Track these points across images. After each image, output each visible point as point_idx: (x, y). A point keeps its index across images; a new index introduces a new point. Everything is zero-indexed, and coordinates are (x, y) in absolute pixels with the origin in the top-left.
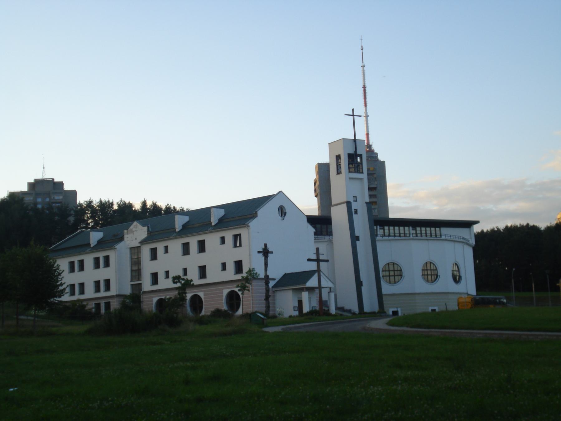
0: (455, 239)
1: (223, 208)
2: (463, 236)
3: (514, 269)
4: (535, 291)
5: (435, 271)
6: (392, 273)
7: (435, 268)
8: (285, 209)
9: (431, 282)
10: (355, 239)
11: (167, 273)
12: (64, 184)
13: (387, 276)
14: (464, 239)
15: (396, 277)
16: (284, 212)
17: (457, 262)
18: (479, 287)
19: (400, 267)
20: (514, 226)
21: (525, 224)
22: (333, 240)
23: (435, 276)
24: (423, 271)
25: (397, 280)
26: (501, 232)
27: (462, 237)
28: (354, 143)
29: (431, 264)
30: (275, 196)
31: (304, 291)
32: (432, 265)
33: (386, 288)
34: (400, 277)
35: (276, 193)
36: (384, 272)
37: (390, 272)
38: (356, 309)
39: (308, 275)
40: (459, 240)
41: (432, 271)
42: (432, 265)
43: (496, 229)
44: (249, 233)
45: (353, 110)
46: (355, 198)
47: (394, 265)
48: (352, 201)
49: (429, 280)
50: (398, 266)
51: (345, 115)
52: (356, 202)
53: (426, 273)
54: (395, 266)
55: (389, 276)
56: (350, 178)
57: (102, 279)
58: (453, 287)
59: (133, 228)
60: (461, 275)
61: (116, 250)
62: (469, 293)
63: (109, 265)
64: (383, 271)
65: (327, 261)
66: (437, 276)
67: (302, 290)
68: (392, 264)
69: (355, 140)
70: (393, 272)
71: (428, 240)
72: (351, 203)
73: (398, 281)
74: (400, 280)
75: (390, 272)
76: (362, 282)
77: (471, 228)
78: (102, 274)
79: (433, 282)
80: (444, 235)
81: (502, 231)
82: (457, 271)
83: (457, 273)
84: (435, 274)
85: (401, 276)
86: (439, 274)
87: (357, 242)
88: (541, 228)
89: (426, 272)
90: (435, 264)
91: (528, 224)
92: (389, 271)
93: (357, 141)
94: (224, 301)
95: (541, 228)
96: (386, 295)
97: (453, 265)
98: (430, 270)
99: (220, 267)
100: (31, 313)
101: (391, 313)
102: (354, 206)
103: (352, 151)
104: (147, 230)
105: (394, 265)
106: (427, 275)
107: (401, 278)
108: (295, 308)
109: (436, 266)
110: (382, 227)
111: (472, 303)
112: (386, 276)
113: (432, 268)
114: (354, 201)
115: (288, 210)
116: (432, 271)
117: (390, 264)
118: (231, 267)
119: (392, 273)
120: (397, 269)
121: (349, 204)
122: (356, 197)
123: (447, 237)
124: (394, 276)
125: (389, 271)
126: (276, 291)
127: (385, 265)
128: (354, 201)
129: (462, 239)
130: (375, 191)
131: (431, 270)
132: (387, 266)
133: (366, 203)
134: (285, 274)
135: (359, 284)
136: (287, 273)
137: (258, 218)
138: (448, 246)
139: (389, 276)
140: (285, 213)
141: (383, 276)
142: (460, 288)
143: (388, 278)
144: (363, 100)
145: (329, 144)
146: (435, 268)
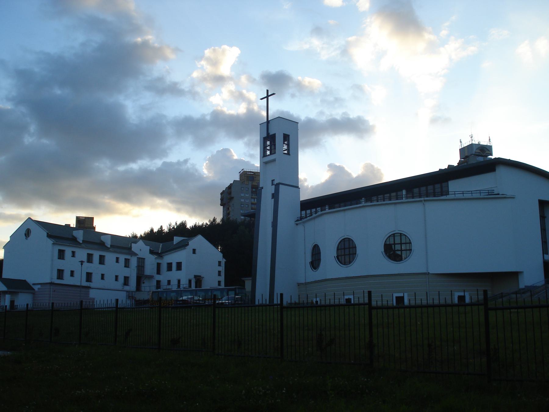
1: (148, 246)
11: (273, 181)
28: (269, 132)
36: (408, 248)
45: (262, 99)
47: (401, 236)
54: (403, 237)
65: (472, 195)
68: (399, 234)
71: (314, 218)
85: (411, 250)
98: (343, 255)
103: (376, 201)
105: (401, 236)
112: (406, 243)
116: (343, 253)
118: (121, 280)
134: (25, 281)
145: (260, 124)
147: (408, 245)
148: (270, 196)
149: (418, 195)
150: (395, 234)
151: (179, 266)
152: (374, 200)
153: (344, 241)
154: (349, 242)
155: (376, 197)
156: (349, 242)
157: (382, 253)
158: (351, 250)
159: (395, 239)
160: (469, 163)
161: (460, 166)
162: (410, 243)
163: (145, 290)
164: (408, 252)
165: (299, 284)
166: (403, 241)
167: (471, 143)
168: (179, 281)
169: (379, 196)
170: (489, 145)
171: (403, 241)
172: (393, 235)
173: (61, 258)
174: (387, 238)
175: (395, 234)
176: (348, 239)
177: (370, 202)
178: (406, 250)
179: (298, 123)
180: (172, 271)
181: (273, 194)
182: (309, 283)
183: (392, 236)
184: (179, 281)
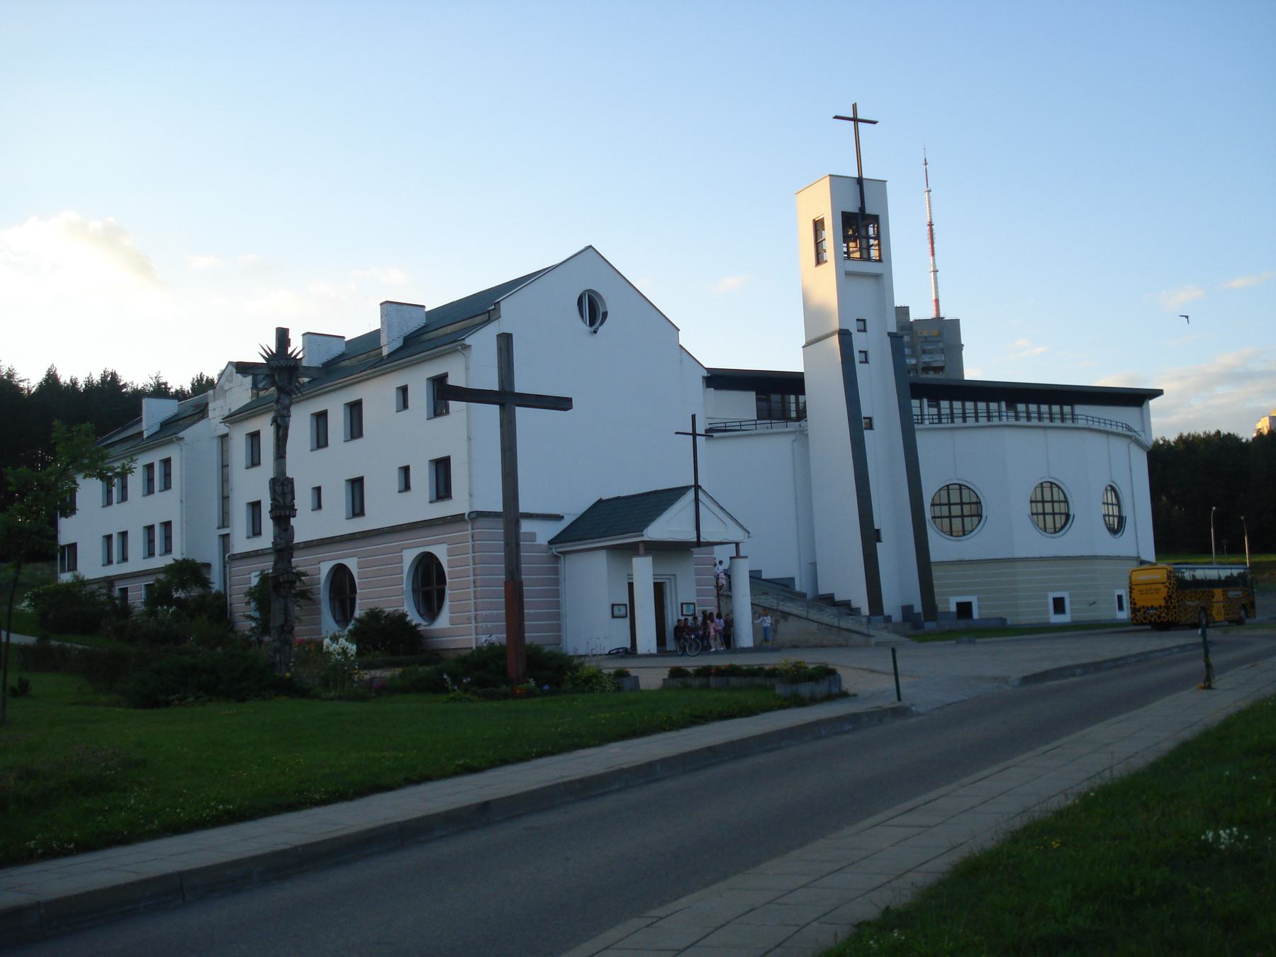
0: (1108, 428)
2: (1127, 423)
3: (1214, 508)
4: (1216, 553)
5: (1062, 504)
6: (956, 510)
7: (1062, 498)
8: (604, 304)
9: (1053, 530)
10: (858, 424)
12: (291, 340)
14: (1129, 429)
15: (967, 520)
16: (601, 311)
17: (1114, 482)
18: (1167, 540)
19: (977, 496)
20: (1194, 437)
21: (1213, 432)
22: (807, 430)
23: (1063, 517)
24: (1034, 504)
25: (968, 527)
26: (1172, 446)
27: (1126, 424)
29: (1051, 488)
31: (638, 555)
32: (1055, 490)
33: (941, 547)
34: (975, 519)
36: (937, 508)
37: (952, 507)
38: (860, 600)
39: (660, 500)
40: (1120, 430)
42: (1055, 490)
43: (1161, 442)
44: (467, 369)
46: (862, 323)
47: (960, 489)
48: (853, 329)
49: (1048, 526)
50: (971, 491)
51: (834, 118)
52: (865, 333)
53: (1040, 511)
54: (965, 492)
55: (950, 517)
56: (849, 274)
57: (157, 521)
58: (1108, 545)
59: (225, 383)
60: (1124, 514)
61: (182, 443)
62: (1144, 557)
64: (933, 505)
66: (1068, 516)
67: (632, 550)
68: (958, 487)
69: (860, 181)
70: (959, 507)
71: (1045, 428)
72: (851, 334)
73: (971, 529)
74: (976, 528)
75: (952, 507)
76: (878, 531)
77: (1144, 406)
78: (164, 507)
79: (1057, 530)
80: (1085, 418)
81: (1173, 444)
82: (1115, 505)
83: (1116, 508)
84: (1063, 511)
85: (980, 516)
86: (1071, 513)
87: (867, 433)
88: (1242, 438)
90: (1063, 487)
91: (1218, 432)
92: (949, 504)
93: (865, 183)
94: (406, 584)
95: (1242, 438)
96: (938, 563)
97: (1106, 490)
99: (395, 479)
100: (30, 610)
101: (953, 608)
102: (859, 341)
103: (853, 207)
104: (250, 386)
105: (960, 489)
106: (1044, 514)
107: (979, 522)
108: (616, 609)
109: (1066, 491)
110: (934, 401)
111: (1170, 584)
112: (941, 517)
113: (1056, 498)
114: (858, 331)
115: (611, 303)
117: (950, 487)
118: (422, 479)
119: (956, 510)
120: (968, 501)
121: (844, 335)
122: (864, 321)
123: (1090, 423)
124: (962, 516)
125: (949, 504)
126: (564, 553)
127: (940, 489)
128: (858, 331)
129: (1125, 429)
130: (941, 373)
131: (1053, 502)
132: (944, 493)
133: (890, 334)
134: (600, 501)
135: (870, 536)
136: (605, 497)
138: (1095, 444)
139: (950, 517)
140: (605, 315)
141: (933, 518)
142: (1123, 545)
143: (946, 521)
144: (930, 246)
146: (1062, 498)
147: (938, 514)
148: (883, 535)
153: (948, 490)
154: (961, 492)
156: (961, 492)
158: (1040, 511)
163: (1112, 504)
164: (937, 501)
172: (946, 488)
176: (475, 514)
178: (940, 505)
179: (886, 181)
181: (879, 540)
183: (1061, 494)
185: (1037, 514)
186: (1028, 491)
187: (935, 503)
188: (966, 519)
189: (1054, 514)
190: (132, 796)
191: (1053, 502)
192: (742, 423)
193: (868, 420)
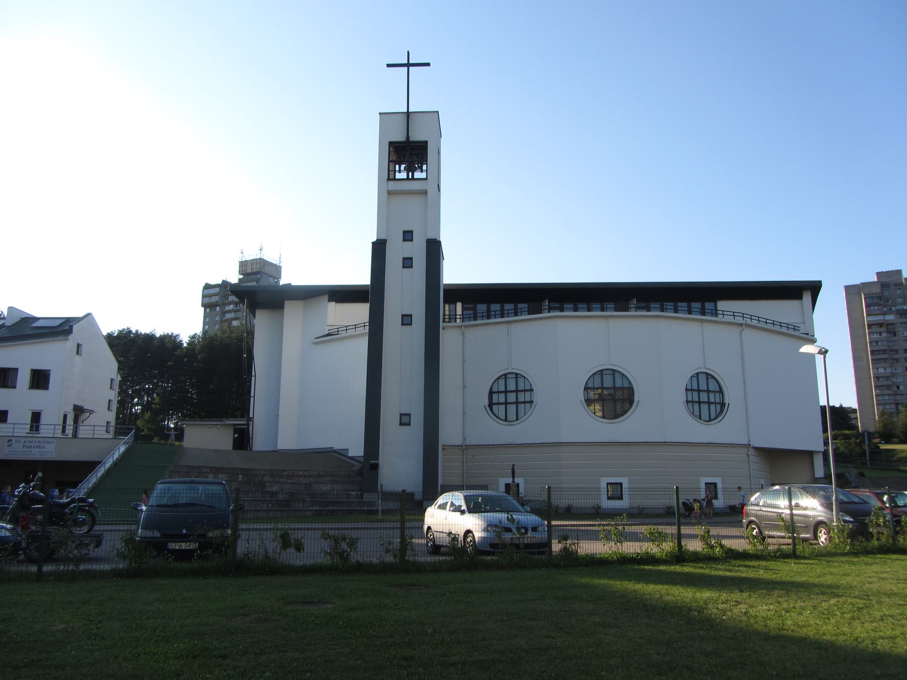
7: (718, 389)
13: (495, 404)
23: (719, 407)
30: (82, 320)
35: (81, 316)
36: (528, 399)
41: (712, 395)
54: (521, 380)
63: (183, 439)
66: (723, 405)
68: (611, 372)
75: (508, 401)
80: (732, 314)
84: (718, 401)
86: (726, 402)
89: (696, 394)
112: (525, 391)
116: (712, 395)
117: (604, 372)
124: (506, 392)
131: (708, 391)
137: (73, 334)
147: (528, 394)
149: (699, 310)
150: (604, 371)
151: (40, 379)
152: (631, 308)
155: (672, 304)
157: (582, 402)
159: (604, 379)
160: (261, 284)
161: (243, 285)
162: (532, 390)
163: (13, 432)
165: (444, 447)
166: (521, 387)
167: (258, 257)
168: (36, 417)
169: (665, 304)
170: (278, 265)
171: (521, 387)
173: (465, 312)
174: (591, 377)
175: (604, 371)
177: (645, 310)
178: (525, 402)
180: (16, 389)
182: (468, 447)
184: (36, 417)
185: (693, 402)
186: (683, 381)
187: (589, 386)
188: (503, 389)
189: (709, 403)
190: (77, 570)
191: (708, 391)
192: (339, 329)
193: (609, 486)
